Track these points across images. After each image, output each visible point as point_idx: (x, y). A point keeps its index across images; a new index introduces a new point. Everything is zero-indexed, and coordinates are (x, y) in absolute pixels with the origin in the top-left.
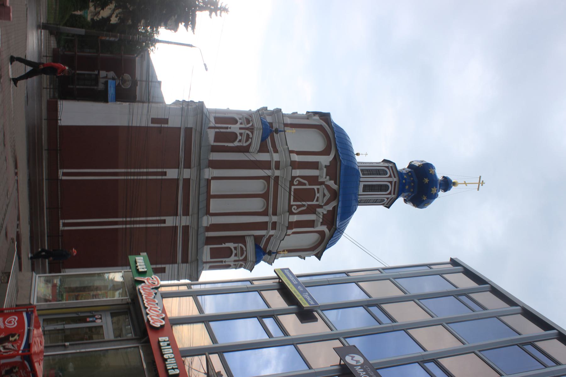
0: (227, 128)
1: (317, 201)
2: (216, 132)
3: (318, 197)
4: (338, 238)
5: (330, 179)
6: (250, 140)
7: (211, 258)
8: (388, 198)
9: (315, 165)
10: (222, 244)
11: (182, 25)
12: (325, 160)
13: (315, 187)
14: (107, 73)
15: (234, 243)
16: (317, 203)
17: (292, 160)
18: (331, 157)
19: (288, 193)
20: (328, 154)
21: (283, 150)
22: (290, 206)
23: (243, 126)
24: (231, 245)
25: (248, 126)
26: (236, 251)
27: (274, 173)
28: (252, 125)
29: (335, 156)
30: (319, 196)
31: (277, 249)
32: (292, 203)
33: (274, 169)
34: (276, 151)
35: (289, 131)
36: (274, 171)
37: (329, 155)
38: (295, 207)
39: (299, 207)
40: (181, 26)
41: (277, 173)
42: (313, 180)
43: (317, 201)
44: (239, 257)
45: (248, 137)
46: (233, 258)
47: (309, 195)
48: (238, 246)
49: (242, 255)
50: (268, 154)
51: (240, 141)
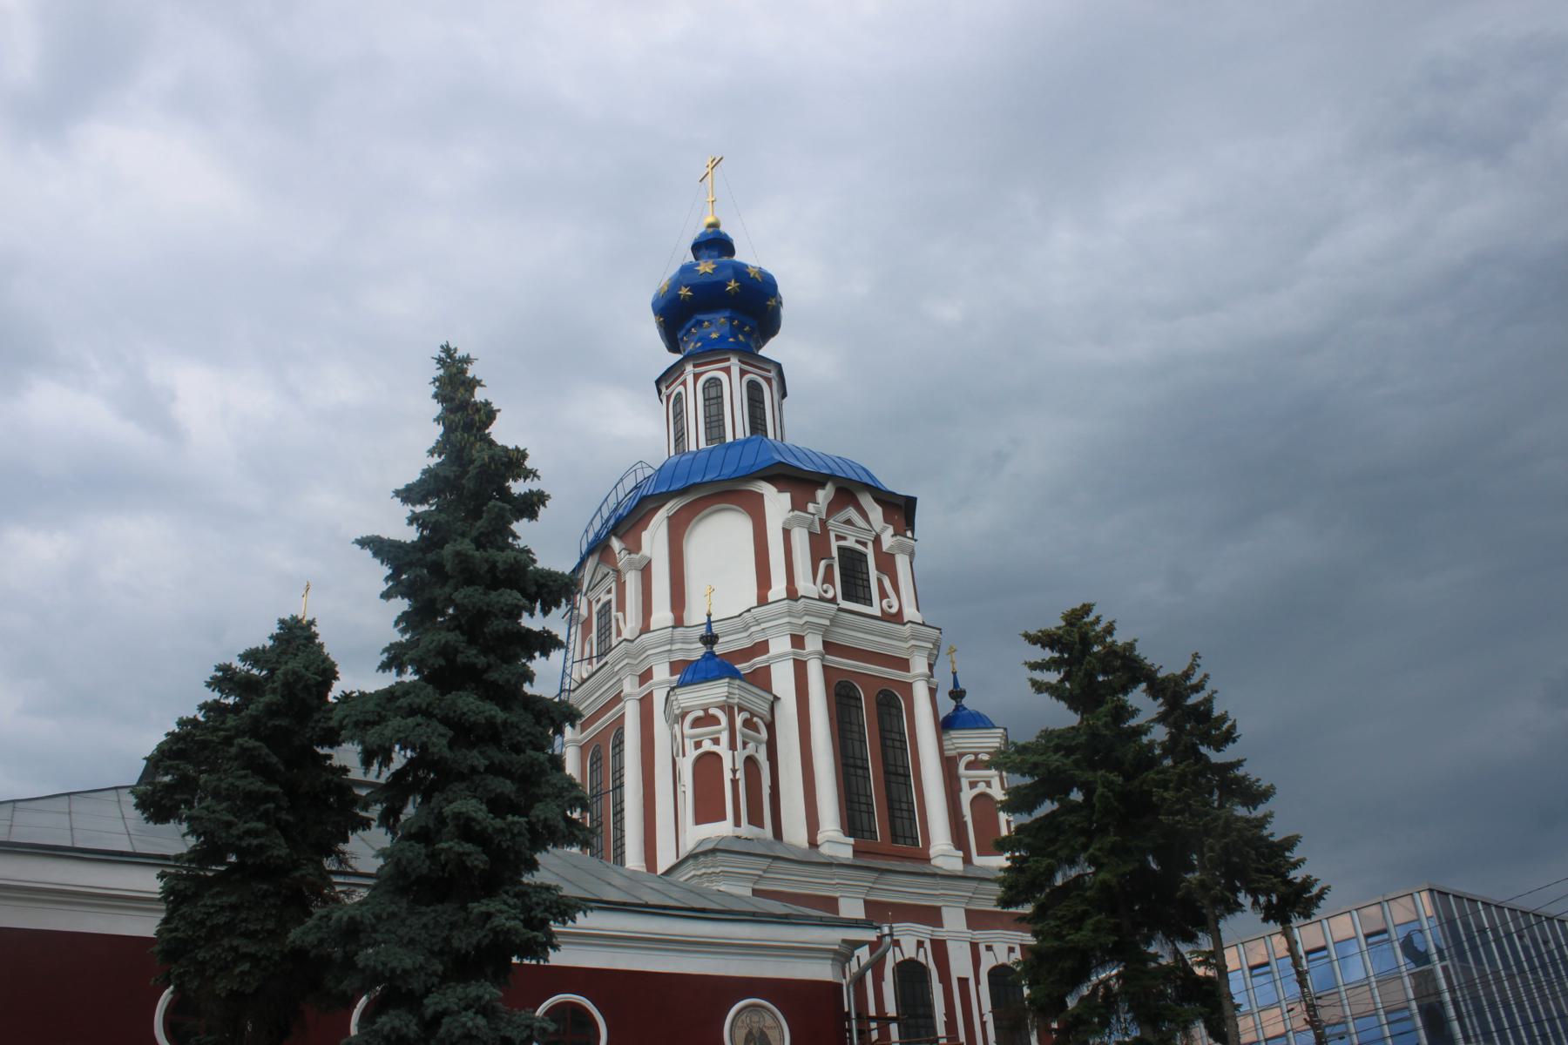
0: (735, 782)
2: (980, 854)
3: (857, 542)
4: (851, 464)
7: (723, 818)
8: (743, 373)
9: (787, 533)
11: (335, 756)
12: (777, 503)
16: (870, 545)
17: (756, 604)
18: (768, 490)
22: (886, 617)
24: (966, 796)
26: (978, 782)
27: (781, 657)
28: (721, 708)
30: (854, 539)
32: (875, 610)
33: (769, 655)
34: (762, 648)
35: (695, 614)
36: (914, 676)
37: (762, 495)
39: (883, 594)
40: (185, 718)
43: (864, 544)
44: (719, 732)
46: (723, 749)
48: (692, 737)
49: (716, 721)
50: (772, 666)
51: (716, 741)
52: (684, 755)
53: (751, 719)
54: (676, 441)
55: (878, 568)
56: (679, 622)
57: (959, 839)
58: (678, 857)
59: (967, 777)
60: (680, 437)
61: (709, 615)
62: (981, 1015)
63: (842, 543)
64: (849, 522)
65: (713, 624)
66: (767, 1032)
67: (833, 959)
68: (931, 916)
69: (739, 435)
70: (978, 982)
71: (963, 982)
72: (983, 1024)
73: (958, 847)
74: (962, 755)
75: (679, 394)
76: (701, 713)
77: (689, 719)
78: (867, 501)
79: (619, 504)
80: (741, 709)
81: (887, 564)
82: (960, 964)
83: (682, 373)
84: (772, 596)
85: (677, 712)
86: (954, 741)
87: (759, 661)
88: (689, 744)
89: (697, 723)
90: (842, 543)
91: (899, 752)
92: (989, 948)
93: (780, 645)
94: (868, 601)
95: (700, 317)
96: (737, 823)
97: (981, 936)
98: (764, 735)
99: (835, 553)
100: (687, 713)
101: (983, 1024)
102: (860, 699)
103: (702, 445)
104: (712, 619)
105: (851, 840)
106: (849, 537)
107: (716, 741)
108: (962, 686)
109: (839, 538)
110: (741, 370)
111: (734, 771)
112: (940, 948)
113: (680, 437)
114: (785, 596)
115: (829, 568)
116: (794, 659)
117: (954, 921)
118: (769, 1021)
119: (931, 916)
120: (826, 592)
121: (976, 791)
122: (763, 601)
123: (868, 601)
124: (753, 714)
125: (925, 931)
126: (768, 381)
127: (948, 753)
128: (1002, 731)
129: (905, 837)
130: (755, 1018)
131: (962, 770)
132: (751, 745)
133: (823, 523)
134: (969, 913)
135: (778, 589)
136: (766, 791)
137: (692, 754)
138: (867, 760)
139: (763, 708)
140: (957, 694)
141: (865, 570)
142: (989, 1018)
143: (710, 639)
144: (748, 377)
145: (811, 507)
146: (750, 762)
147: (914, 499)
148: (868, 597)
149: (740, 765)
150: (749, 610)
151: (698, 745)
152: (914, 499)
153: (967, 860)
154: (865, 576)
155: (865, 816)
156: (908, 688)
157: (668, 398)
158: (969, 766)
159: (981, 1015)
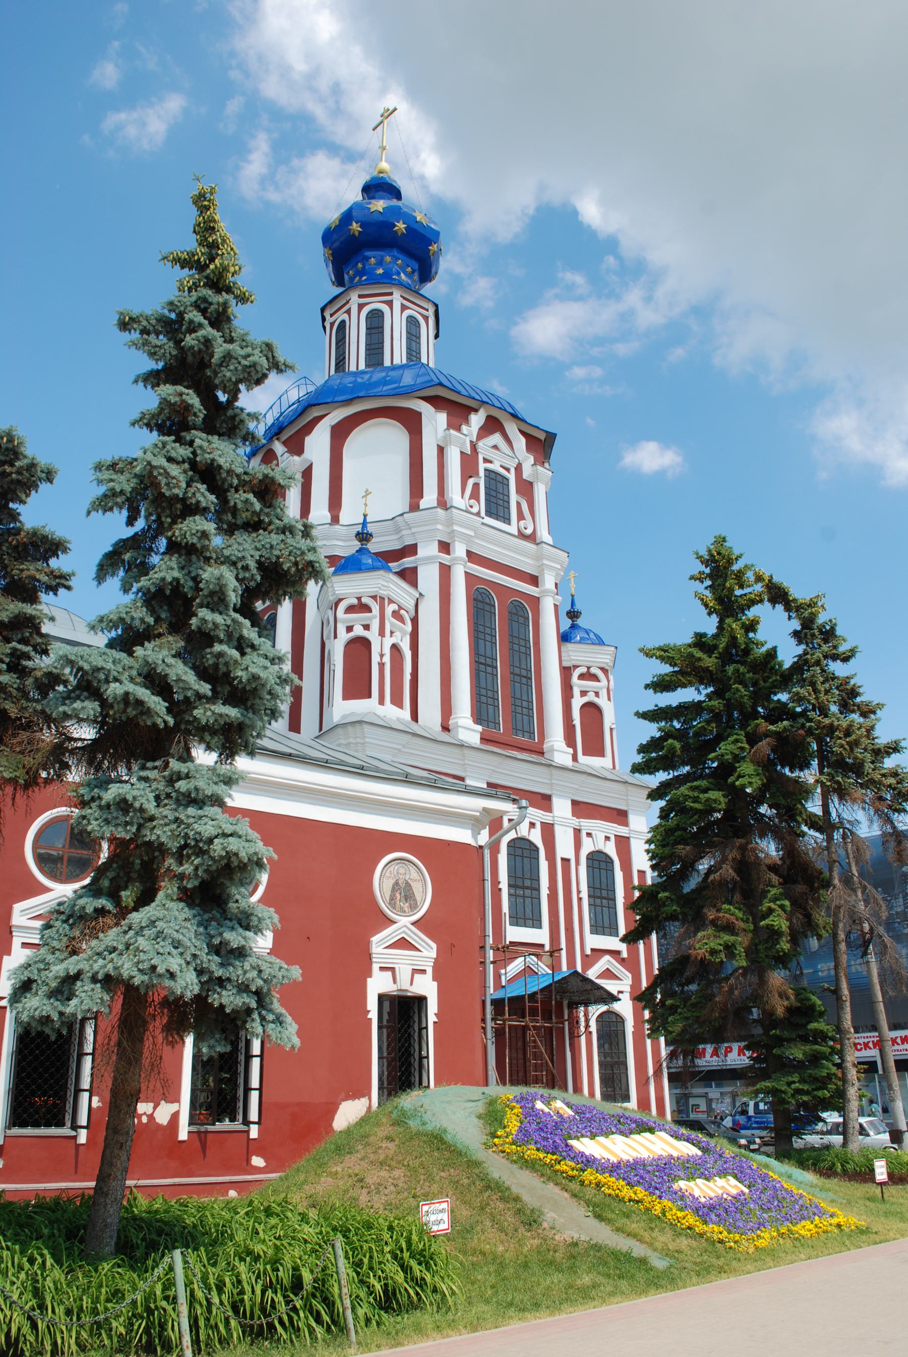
0: (382, 665)
1: (508, 470)
2: (584, 754)
5: (467, 422)
6: (593, 670)
7: (370, 696)
8: (404, 308)
9: (441, 450)
10: (371, 1019)
13: (482, 466)
14: (375, 967)
15: (572, 697)
16: (513, 471)
18: (425, 408)
19: (439, 510)
20: (419, 415)
21: (325, 545)
22: (522, 536)
23: (375, 626)
24: (577, 702)
25: (375, 608)
27: (429, 560)
29: (426, 399)
31: (361, 394)
34: (411, 550)
35: (350, 514)
37: (420, 414)
38: (522, 523)
39: (521, 517)
41: (459, 550)
42: (469, 463)
43: (508, 470)
45: (588, 676)
46: (372, 635)
47: (496, 483)
48: (344, 621)
51: (367, 627)
52: (335, 637)
53: (399, 610)
54: (336, 365)
55: (518, 492)
56: (335, 520)
57: (570, 740)
58: (321, 729)
59: (579, 686)
60: (341, 362)
61: (365, 516)
62: (579, 892)
63: (489, 466)
64: (495, 447)
65: (368, 525)
66: (412, 884)
67: (473, 825)
68: (544, 801)
69: (397, 361)
70: (578, 863)
71: (566, 861)
72: (580, 899)
73: (569, 745)
74: (576, 667)
75: (343, 322)
76: (355, 602)
77: (342, 607)
78: (512, 428)
79: (282, 414)
80: (391, 601)
81: (526, 488)
82: (564, 847)
83: (348, 302)
84: (423, 504)
85: (331, 598)
86: (571, 653)
87: (408, 562)
88: (341, 629)
89: (350, 609)
90: (489, 466)
91: (523, 656)
92: (589, 835)
93: (428, 550)
94: (507, 521)
95: (368, 254)
96: (381, 701)
97: (587, 824)
98: (409, 627)
99: (482, 473)
100: (340, 600)
101: (580, 899)
102: (494, 606)
103: (362, 366)
104: (368, 520)
105: (479, 728)
106: (495, 462)
107: (367, 627)
108: (578, 607)
109: (486, 460)
110: (402, 305)
111: (382, 656)
112: (548, 831)
113: (341, 362)
114: (436, 505)
115: (476, 485)
116: (440, 563)
117: (562, 808)
118: (414, 874)
119: (544, 801)
120: (471, 507)
121: (585, 699)
122: (414, 507)
123: (507, 521)
124: (400, 608)
125: (535, 814)
126: (426, 318)
127: (565, 664)
128: (613, 649)
129: (523, 731)
130: (402, 871)
131: (575, 679)
132: (398, 634)
133: (474, 446)
134: (575, 803)
135: (430, 497)
136: (407, 677)
137: (344, 637)
138: (496, 660)
139: (410, 604)
140: (573, 615)
141: (506, 493)
142: (585, 895)
143: (364, 537)
144: (407, 312)
145: (464, 428)
146: (395, 648)
147: (556, 435)
148: (506, 516)
149: (387, 651)
150: (402, 515)
151: (349, 629)
152: (556, 435)
153: (575, 758)
154: (506, 498)
155: (491, 708)
156: (535, 602)
157: (332, 325)
158: (582, 677)
159: (579, 892)
